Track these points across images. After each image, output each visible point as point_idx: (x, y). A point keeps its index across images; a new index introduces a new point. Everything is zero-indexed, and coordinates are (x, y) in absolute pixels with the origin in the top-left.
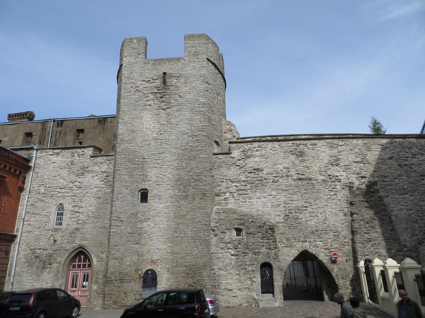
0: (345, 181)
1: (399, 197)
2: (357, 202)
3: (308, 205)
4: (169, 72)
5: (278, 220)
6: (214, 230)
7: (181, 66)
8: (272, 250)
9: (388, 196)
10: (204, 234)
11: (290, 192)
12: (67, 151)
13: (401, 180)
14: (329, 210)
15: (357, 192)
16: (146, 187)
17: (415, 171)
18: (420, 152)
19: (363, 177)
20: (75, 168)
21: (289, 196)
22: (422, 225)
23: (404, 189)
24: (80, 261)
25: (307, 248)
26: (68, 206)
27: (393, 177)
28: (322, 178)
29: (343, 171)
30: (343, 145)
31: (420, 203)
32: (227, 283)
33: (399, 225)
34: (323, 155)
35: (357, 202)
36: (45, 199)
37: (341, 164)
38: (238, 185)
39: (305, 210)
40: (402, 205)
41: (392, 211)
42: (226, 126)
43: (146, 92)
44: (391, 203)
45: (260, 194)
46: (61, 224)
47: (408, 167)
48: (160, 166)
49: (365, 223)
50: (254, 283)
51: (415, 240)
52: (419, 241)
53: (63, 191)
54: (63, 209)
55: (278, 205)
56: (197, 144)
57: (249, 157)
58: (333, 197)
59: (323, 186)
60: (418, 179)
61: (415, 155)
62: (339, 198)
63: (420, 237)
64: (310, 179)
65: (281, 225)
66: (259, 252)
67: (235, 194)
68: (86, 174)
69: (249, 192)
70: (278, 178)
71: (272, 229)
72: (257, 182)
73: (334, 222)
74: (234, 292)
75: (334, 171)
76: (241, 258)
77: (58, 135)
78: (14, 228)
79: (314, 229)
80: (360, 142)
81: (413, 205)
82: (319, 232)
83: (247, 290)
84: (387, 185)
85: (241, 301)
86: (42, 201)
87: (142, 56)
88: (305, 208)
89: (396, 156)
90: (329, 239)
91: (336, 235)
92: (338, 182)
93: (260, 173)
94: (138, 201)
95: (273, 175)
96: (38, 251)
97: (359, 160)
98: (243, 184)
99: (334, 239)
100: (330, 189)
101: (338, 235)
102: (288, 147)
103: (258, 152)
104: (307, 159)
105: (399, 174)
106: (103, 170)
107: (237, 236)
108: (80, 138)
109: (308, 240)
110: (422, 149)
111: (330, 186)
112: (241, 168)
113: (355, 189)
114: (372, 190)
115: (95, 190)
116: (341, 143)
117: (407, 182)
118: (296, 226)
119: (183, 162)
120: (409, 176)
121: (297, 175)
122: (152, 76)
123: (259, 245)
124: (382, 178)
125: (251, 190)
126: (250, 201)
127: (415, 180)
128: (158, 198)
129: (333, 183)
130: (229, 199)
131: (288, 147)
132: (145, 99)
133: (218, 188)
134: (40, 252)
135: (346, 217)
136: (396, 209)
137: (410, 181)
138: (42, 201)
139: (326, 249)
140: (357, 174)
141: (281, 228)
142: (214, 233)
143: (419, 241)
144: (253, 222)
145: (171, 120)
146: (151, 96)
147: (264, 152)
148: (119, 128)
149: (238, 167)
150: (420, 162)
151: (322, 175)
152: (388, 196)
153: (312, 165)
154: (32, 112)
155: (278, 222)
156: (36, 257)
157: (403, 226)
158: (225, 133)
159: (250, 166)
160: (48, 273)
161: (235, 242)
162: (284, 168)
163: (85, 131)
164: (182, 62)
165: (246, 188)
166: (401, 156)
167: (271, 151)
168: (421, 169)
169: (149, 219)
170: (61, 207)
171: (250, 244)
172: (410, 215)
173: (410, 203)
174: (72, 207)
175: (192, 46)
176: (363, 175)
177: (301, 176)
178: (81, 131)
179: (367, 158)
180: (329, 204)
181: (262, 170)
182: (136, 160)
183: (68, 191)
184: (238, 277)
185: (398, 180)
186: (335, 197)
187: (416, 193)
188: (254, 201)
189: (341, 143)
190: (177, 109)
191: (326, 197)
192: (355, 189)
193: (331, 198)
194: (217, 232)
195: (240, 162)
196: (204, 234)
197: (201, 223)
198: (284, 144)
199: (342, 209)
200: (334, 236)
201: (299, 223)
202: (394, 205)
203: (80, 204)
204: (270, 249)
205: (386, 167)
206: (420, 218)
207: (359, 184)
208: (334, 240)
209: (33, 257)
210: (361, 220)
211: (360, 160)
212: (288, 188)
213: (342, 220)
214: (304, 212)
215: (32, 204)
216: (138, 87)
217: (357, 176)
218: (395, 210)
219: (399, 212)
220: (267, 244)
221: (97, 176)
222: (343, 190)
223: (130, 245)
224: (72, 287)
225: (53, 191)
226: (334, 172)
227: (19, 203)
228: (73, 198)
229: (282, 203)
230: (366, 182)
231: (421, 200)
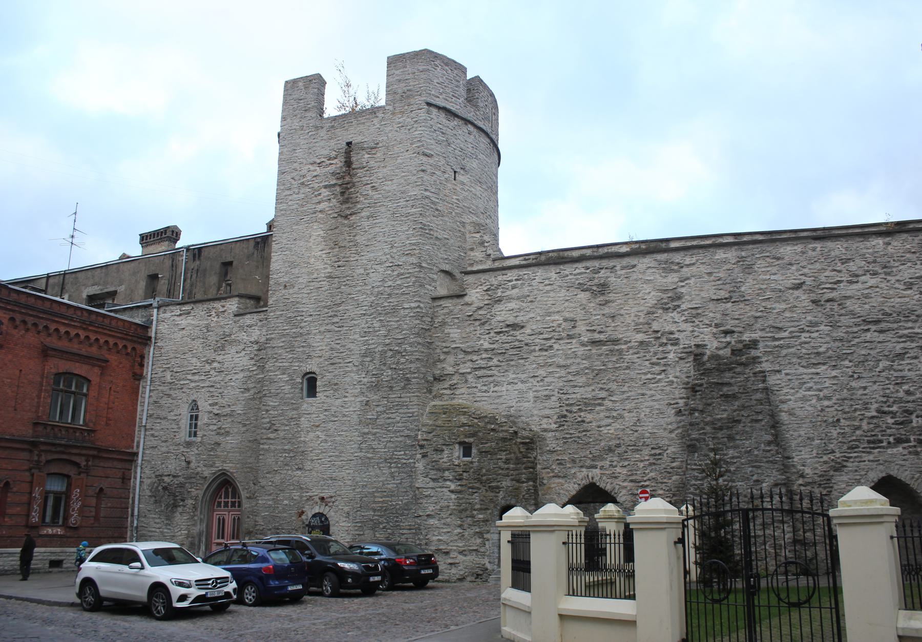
0: (688, 342)
1: (805, 371)
2: (705, 386)
3: (603, 394)
4: (356, 139)
5: (545, 426)
6: (422, 447)
7: (378, 126)
8: (523, 482)
9: (779, 371)
10: (405, 454)
11: (573, 369)
12: (200, 305)
13: (815, 335)
14: (646, 404)
15: (708, 365)
16: (315, 369)
17: (852, 313)
18: (871, 268)
19: (726, 333)
20: (212, 337)
21: (570, 378)
22: (847, 429)
23: (818, 354)
24: (227, 497)
25: (596, 479)
26: (204, 405)
27: (796, 329)
28: (640, 337)
29: (686, 321)
30: (693, 264)
31: (854, 384)
32: (439, 540)
33: (795, 431)
34: (647, 288)
35: (705, 386)
36: (172, 392)
37: (684, 307)
38: (475, 358)
39: (600, 405)
40: (810, 389)
41: (783, 402)
42: (474, 235)
43: (316, 186)
44: (783, 384)
45: (514, 376)
46: (195, 435)
47: (836, 304)
48: (337, 329)
49: (715, 428)
50: (487, 543)
51: (825, 462)
52: (833, 464)
53: (196, 378)
54: (197, 409)
55: (548, 397)
56: (399, 282)
57: (499, 301)
58: (659, 377)
59: (642, 354)
60: (855, 329)
61: (857, 276)
62: (671, 378)
63: (838, 455)
64: (616, 341)
65: (550, 434)
66: (498, 487)
67: (469, 377)
68: (228, 348)
69: (495, 372)
70: (553, 341)
71: (531, 443)
72: (511, 352)
73: (654, 427)
74: (451, 556)
75: (665, 322)
76: (467, 496)
77: (194, 276)
78: (133, 441)
79: (613, 443)
80: (731, 255)
81: (835, 387)
82: (623, 448)
83: (474, 553)
84: (781, 347)
85: (461, 573)
86: (169, 396)
87: (312, 114)
88: (600, 401)
89: (809, 281)
90: (642, 461)
91: (655, 455)
92: (672, 344)
93: (518, 333)
94: (302, 393)
95: (541, 337)
96: (166, 479)
97: (723, 294)
98: (484, 356)
99: (652, 461)
100: (654, 360)
101: (660, 454)
102: (575, 275)
103: (516, 290)
104: (612, 299)
105: (811, 322)
106: (252, 340)
107: (464, 456)
108: (228, 278)
109: (600, 464)
110: (875, 262)
111: (655, 354)
112: (483, 324)
113: (706, 358)
114: (744, 359)
115: (241, 375)
116: (688, 260)
117: (828, 339)
118: (579, 437)
119: (375, 318)
120: (834, 326)
121: (589, 334)
122: (325, 152)
123: (499, 474)
124: (772, 332)
125: (498, 369)
126: (496, 389)
127: (847, 332)
128: (332, 389)
129: (661, 349)
130: (459, 386)
131: (575, 275)
132: (315, 200)
133: (440, 366)
134: (169, 481)
135: (679, 418)
136: (792, 398)
137: (835, 335)
138: (169, 396)
139: (632, 481)
140: (716, 325)
141: (551, 442)
142: (422, 451)
143: (833, 464)
144: (493, 430)
145: (357, 238)
146: (325, 193)
147: (526, 290)
148: (273, 260)
149: (477, 323)
150: (866, 292)
151: (638, 331)
152: (779, 371)
153: (622, 312)
154: (176, 227)
155: (545, 430)
156: (165, 488)
157: (802, 433)
158: (472, 249)
159: (499, 318)
160: (181, 513)
161: (457, 469)
162: (565, 320)
163: (234, 264)
164: (380, 115)
165: (491, 364)
166: (823, 279)
167: (541, 287)
168: (867, 306)
169: (318, 426)
170: (194, 406)
171: (484, 471)
172: (822, 410)
173: (827, 385)
174: (210, 405)
175: (400, 81)
176: (728, 327)
177: (597, 336)
178: (228, 265)
179: (743, 289)
180: (649, 393)
181: (523, 327)
182: (299, 318)
183: (203, 378)
184: (459, 530)
185: (807, 335)
186: (663, 376)
187: (846, 363)
188: (504, 389)
189: (688, 260)
190: (368, 214)
191: (643, 377)
192: (706, 358)
193: (654, 378)
194: (429, 450)
195: (481, 312)
196: (405, 454)
197: (402, 434)
198: (568, 269)
199: (673, 402)
200: (651, 455)
201: (584, 431)
202: (791, 388)
203: (220, 401)
204: (518, 481)
205: (783, 306)
206: (844, 416)
207: (717, 348)
208: (651, 464)
209: (160, 488)
210: (707, 424)
211: (727, 296)
212: (569, 362)
213: (671, 424)
214: (598, 408)
215: (156, 402)
216: (304, 176)
217: (715, 330)
218: (790, 400)
219: (799, 404)
220: (515, 473)
221: (244, 349)
222: (682, 361)
223: (290, 472)
224: (218, 538)
225: (183, 379)
226: (665, 324)
227: (137, 400)
228: (211, 389)
229: (556, 393)
230: (733, 343)
231: (856, 376)
